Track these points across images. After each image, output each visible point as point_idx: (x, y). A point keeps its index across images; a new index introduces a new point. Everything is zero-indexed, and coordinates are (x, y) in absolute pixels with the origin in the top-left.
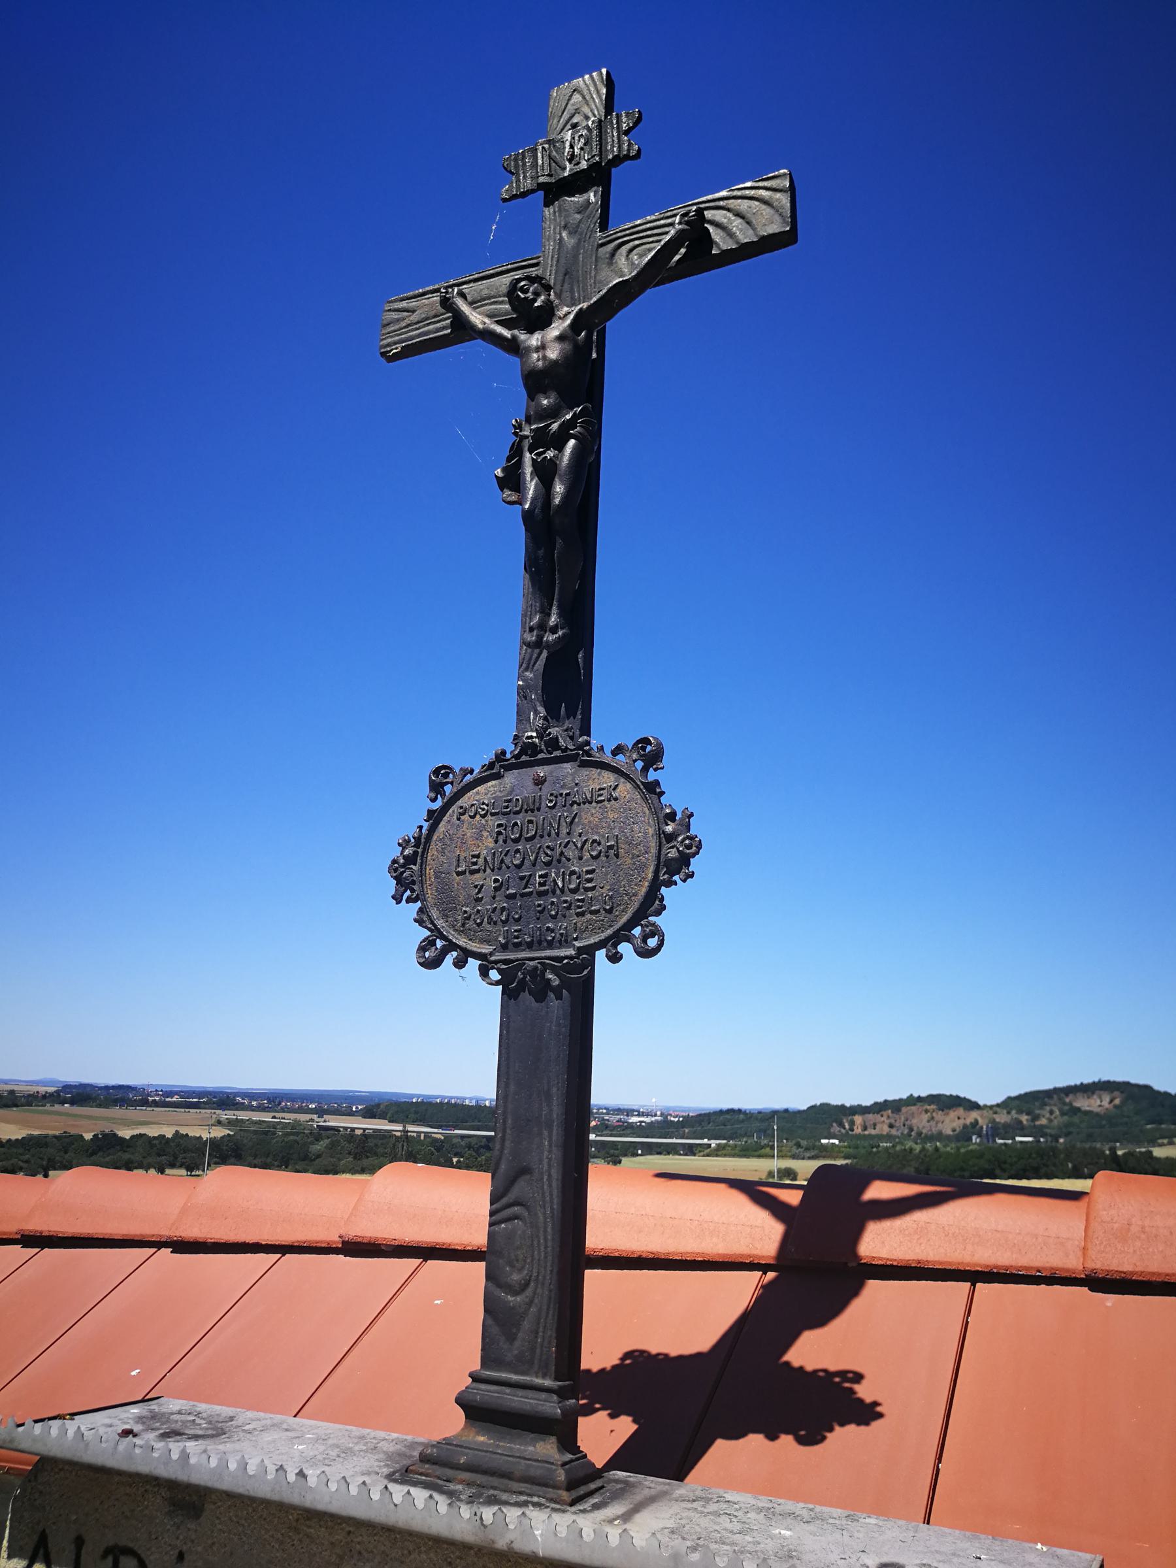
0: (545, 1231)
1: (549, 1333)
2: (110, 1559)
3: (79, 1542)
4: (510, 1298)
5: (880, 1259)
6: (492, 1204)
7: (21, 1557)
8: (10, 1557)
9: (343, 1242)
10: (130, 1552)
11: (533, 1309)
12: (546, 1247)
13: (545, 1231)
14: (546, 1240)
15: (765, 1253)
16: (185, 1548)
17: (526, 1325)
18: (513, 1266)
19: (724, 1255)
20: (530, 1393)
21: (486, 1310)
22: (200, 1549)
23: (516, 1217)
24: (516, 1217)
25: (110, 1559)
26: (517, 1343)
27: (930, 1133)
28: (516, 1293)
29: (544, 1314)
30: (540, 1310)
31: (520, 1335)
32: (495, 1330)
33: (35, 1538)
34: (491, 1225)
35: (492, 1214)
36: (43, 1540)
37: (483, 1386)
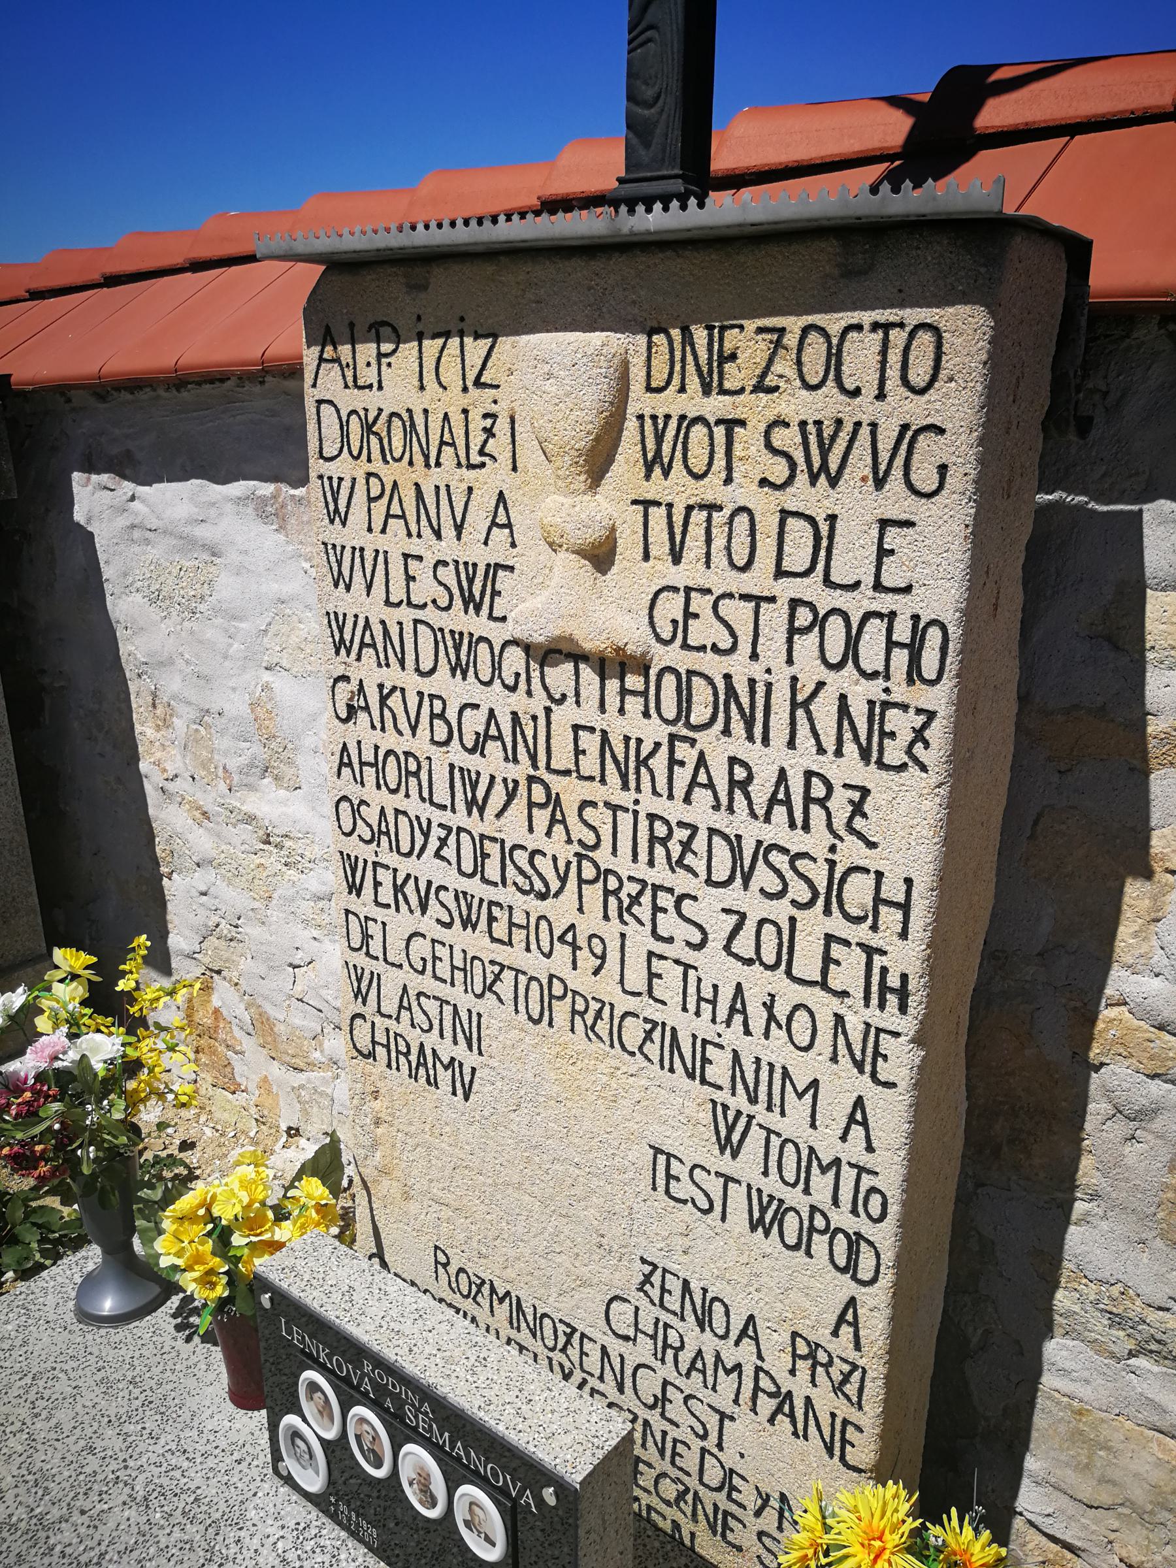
0: (672, 46)
1: (676, 132)
2: (373, 331)
3: (352, 325)
4: (646, 112)
5: (993, 127)
6: (630, 33)
7: (316, 345)
8: (309, 347)
9: (542, 203)
10: (385, 324)
11: (664, 116)
12: (673, 59)
13: (672, 46)
14: (673, 53)
15: (893, 144)
16: (421, 313)
17: (659, 131)
18: (648, 84)
19: (858, 152)
20: (665, 182)
21: (628, 127)
22: (430, 310)
23: (649, 40)
24: (649, 40)
25: (373, 331)
26: (653, 148)
27: (386, 347)
28: (651, 106)
29: (671, 119)
30: (669, 116)
31: (655, 141)
32: (635, 141)
33: (323, 330)
34: (629, 53)
35: (630, 42)
36: (328, 330)
37: (627, 186)
